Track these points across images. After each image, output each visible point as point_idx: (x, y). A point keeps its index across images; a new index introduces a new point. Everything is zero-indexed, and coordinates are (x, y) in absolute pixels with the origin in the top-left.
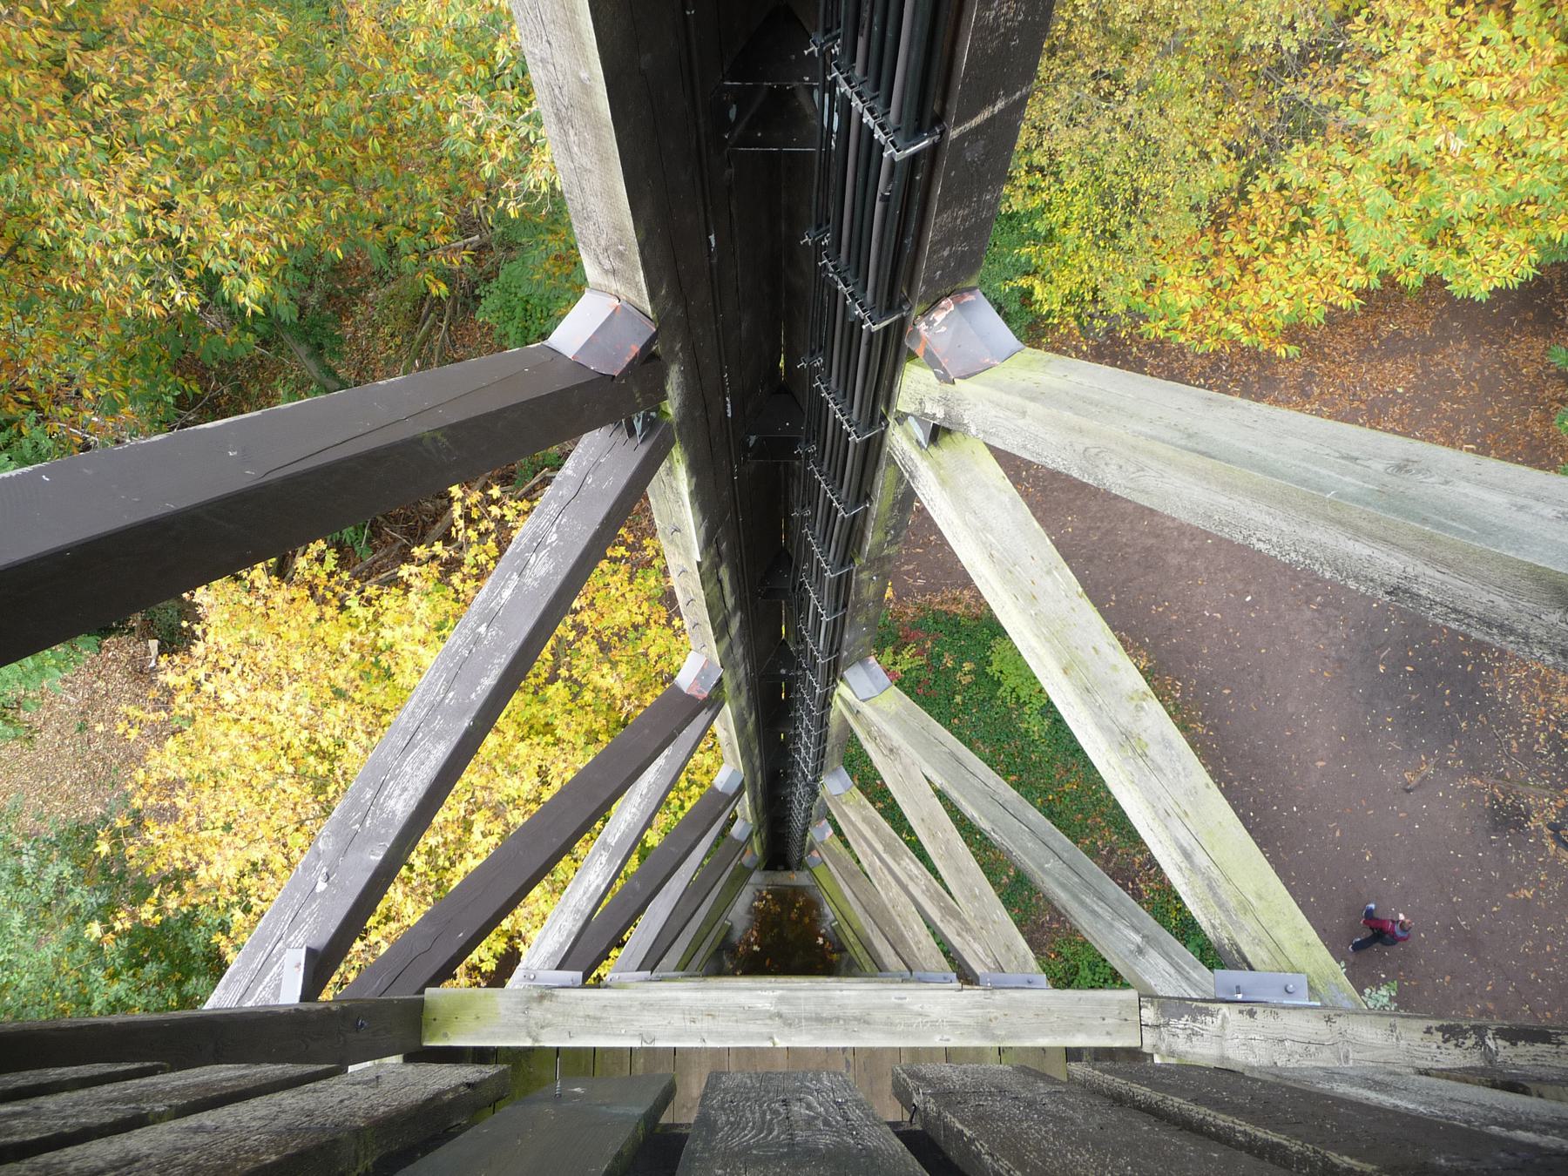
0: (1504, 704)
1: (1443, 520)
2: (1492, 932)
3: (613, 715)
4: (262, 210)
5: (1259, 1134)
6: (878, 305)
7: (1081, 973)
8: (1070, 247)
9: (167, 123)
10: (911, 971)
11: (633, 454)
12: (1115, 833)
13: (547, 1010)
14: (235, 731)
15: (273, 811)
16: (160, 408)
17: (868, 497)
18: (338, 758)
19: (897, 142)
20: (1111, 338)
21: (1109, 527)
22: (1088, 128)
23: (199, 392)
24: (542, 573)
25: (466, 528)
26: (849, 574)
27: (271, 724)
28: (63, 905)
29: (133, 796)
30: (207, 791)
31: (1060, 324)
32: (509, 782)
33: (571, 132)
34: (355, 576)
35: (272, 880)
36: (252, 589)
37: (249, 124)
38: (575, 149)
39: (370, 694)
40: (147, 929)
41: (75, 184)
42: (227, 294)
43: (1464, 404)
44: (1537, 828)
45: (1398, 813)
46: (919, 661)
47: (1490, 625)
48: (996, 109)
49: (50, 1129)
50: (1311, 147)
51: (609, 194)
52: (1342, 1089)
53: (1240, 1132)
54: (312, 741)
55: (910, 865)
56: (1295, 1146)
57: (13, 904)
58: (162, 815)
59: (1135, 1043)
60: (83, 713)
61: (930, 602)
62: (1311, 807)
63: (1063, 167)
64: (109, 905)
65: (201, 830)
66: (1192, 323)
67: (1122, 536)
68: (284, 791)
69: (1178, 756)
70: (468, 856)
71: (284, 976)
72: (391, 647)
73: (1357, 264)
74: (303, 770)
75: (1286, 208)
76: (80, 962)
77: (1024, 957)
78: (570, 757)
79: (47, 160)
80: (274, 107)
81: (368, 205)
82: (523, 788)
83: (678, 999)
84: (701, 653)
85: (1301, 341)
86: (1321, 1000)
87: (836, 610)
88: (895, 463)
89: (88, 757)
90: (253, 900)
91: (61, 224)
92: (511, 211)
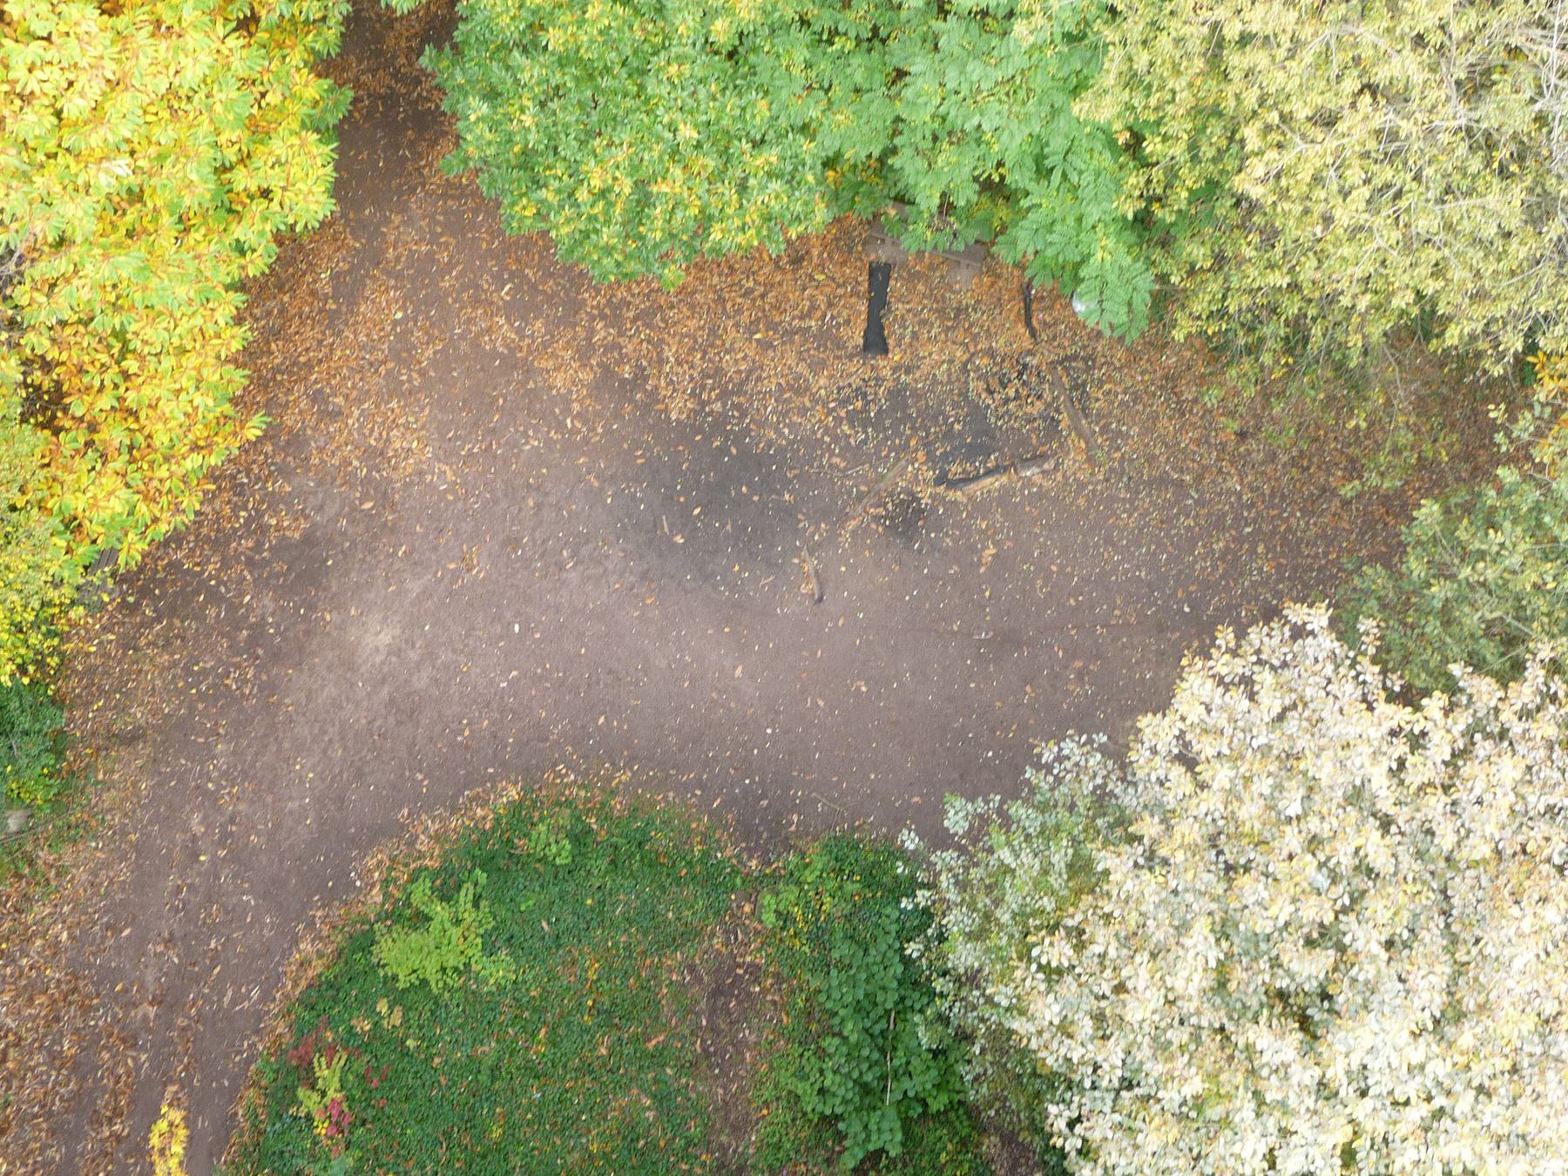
0: (790, 443)
21: (336, 728)
43: (458, 263)
46: (341, 1059)
61: (286, 996)
62: (777, 713)
67: (358, 721)
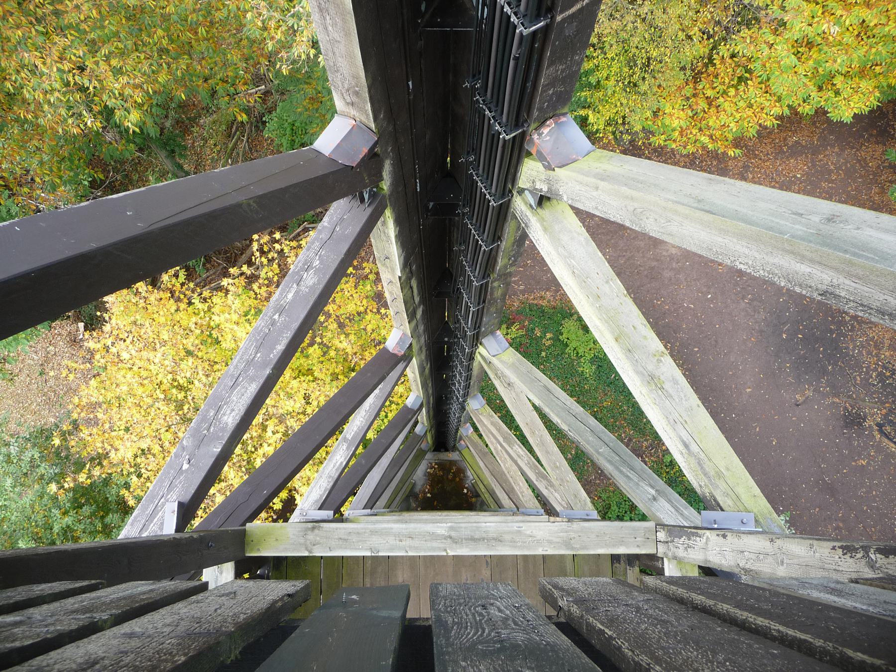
0: (853, 356)
1: (856, 251)
2: (843, 484)
3: (346, 364)
4: (137, 70)
5: (790, 632)
6: (509, 124)
7: (612, 508)
8: (610, 92)
9: (79, 18)
10: (518, 509)
11: (363, 213)
12: (632, 430)
13: (317, 535)
14: (129, 375)
15: (153, 420)
16: (81, 188)
17: (499, 238)
18: (189, 390)
19: (525, 23)
20: (633, 146)
22: (621, 21)
23: (103, 178)
24: (311, 283)
25: (261, 257)
26: (487, 283)
27: (151, 371)
28: (35, 474)
29: (73, 412)
30: (115, 409)
31: (603, 137)
32: (287, 403)
33: (328, 18)
34: (197, 285)
35: (153, 459)
36: (137, 293)
37: (128, 19)
38: (330, 28)
39: (207, 353)
40: (83, 487)
41: (26, 55)
42: (118, 120)
43: (835, 184)
44: (870, 426)
45: (792, 417)
46: (521, 332)
47: (883, 314)
48: (585, 3)
49: (38, 635)
50: (752, 31)
51: (350, 56)
52: (815, 595)
53: (774, 630)
54: (174, 380)
55: (519, 450)
56: (819, 643)
57: (6, 474)
58: (89, 423)
59: (653, 551)
60: (42, 365)
62: (743, 415)
63: (606, 44)
64: (61, 473)
65: (112, 431)
66: (679, 136)
67: (638, 261)
68: (159, 409)
69: (682, 388)
70: (265, 445)
71: (165, 518)
72: (219, 326)
73: (776, 101)
74: (169, 396)
75: (736, 68)
76: (46, 505)
77: (584, 501)
78: (322, 388)
79: (9, 41)
80: (142, 8)
81: (200, 68)
82: (295, 406)
83: (392, 529)
84: (400, 329)
85: (742, 147)
86: (762, 527)
87: (479, 304)
88: (516, 218)
89: (46, 390)
90: (143, 471)
91: (19, 79)
92: (284, 71)
